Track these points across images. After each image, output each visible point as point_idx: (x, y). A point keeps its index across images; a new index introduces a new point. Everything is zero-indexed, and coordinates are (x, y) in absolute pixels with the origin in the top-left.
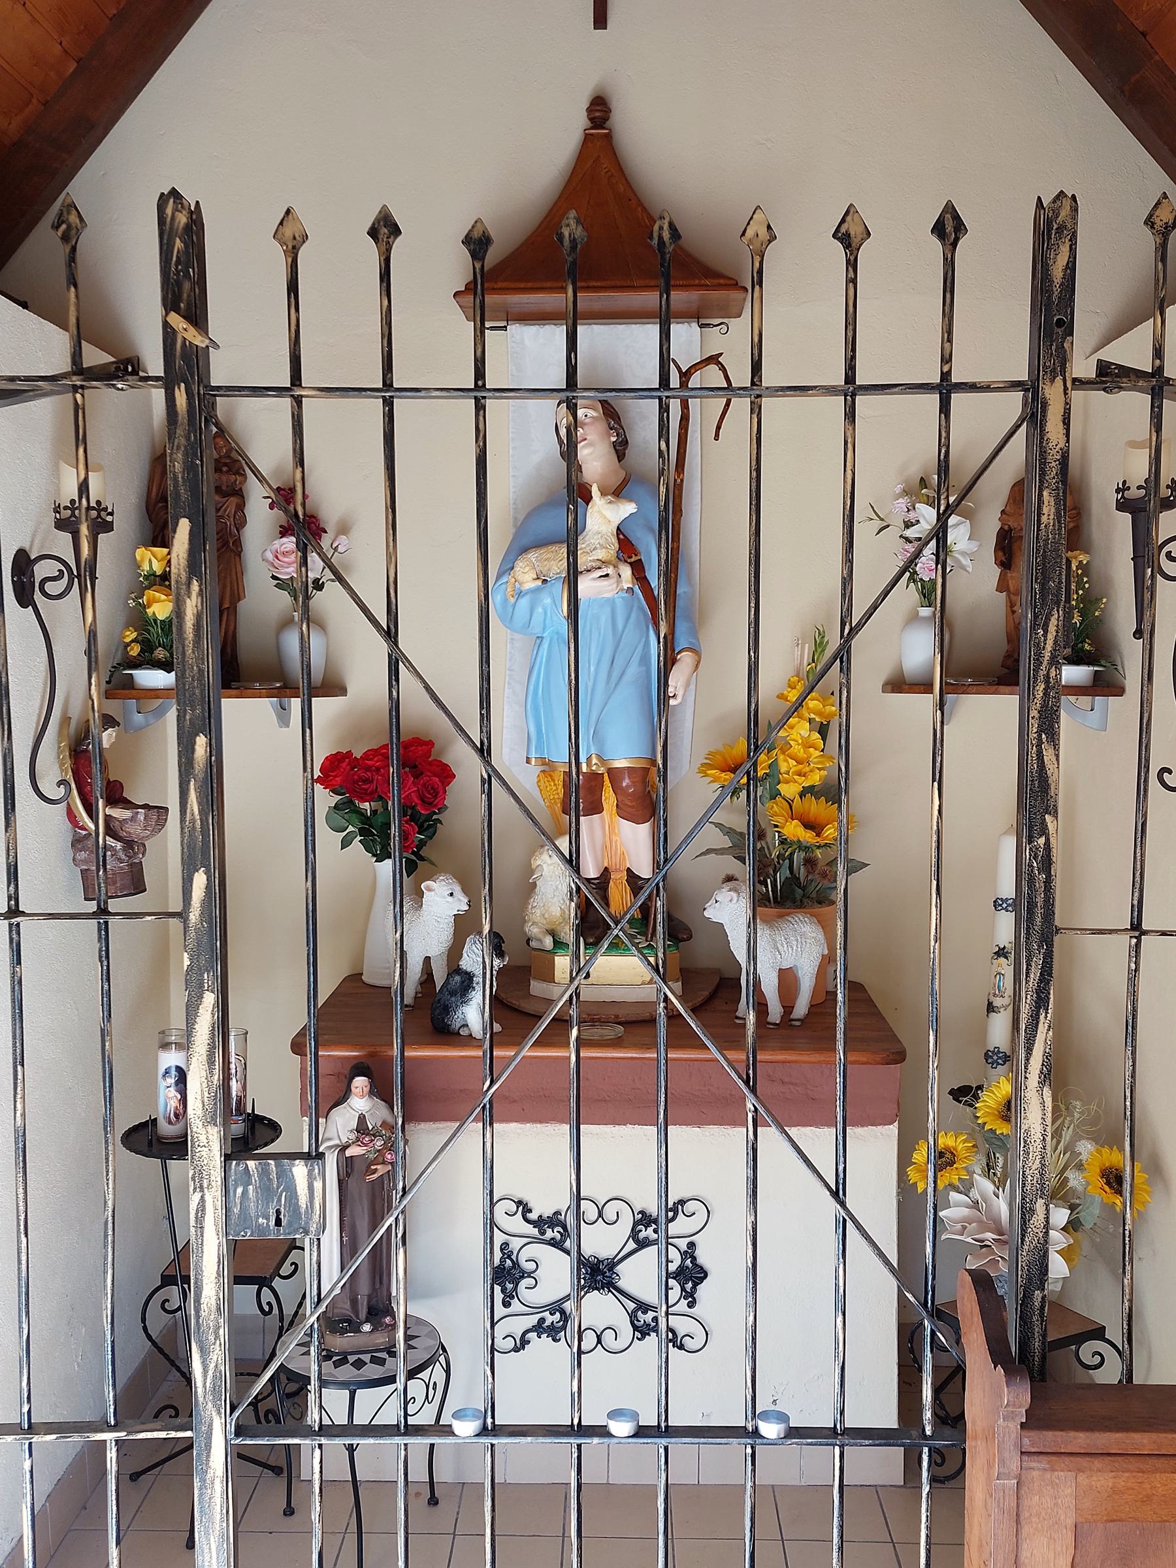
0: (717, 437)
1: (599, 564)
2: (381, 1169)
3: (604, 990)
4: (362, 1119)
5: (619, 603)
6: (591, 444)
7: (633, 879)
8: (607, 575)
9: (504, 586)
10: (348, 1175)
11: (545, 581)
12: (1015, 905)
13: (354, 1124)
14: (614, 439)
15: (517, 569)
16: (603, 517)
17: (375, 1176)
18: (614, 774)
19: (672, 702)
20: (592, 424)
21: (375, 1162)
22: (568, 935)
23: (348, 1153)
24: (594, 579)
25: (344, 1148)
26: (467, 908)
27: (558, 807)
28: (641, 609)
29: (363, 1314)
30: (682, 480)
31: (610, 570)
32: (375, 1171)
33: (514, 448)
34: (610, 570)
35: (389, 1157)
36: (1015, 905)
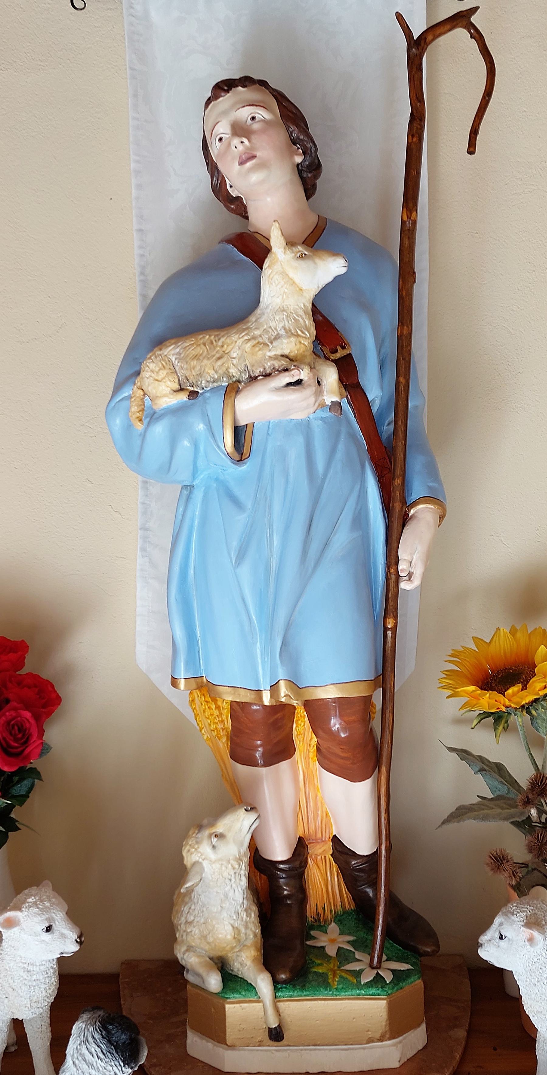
0: (471, 149)
1: (284, 363)
5: (318, 428)
6: (263, 166)
7: (340, 850)
8: (299, 382)
9: (126, 403)
11: (193, 395)
14: (299, 159)
15: (145, 374)
16: (292, 283)
18: (317, 711)
19: (403, 585)
20: (263, 131)
22: (247, 963)
24: (277, 389)
26: (75, 948)
27: (223, 745)
28: (352, 436)
30: (415, 223)
31: (304, 374)
33: (139, 187)
34: (304, 374)
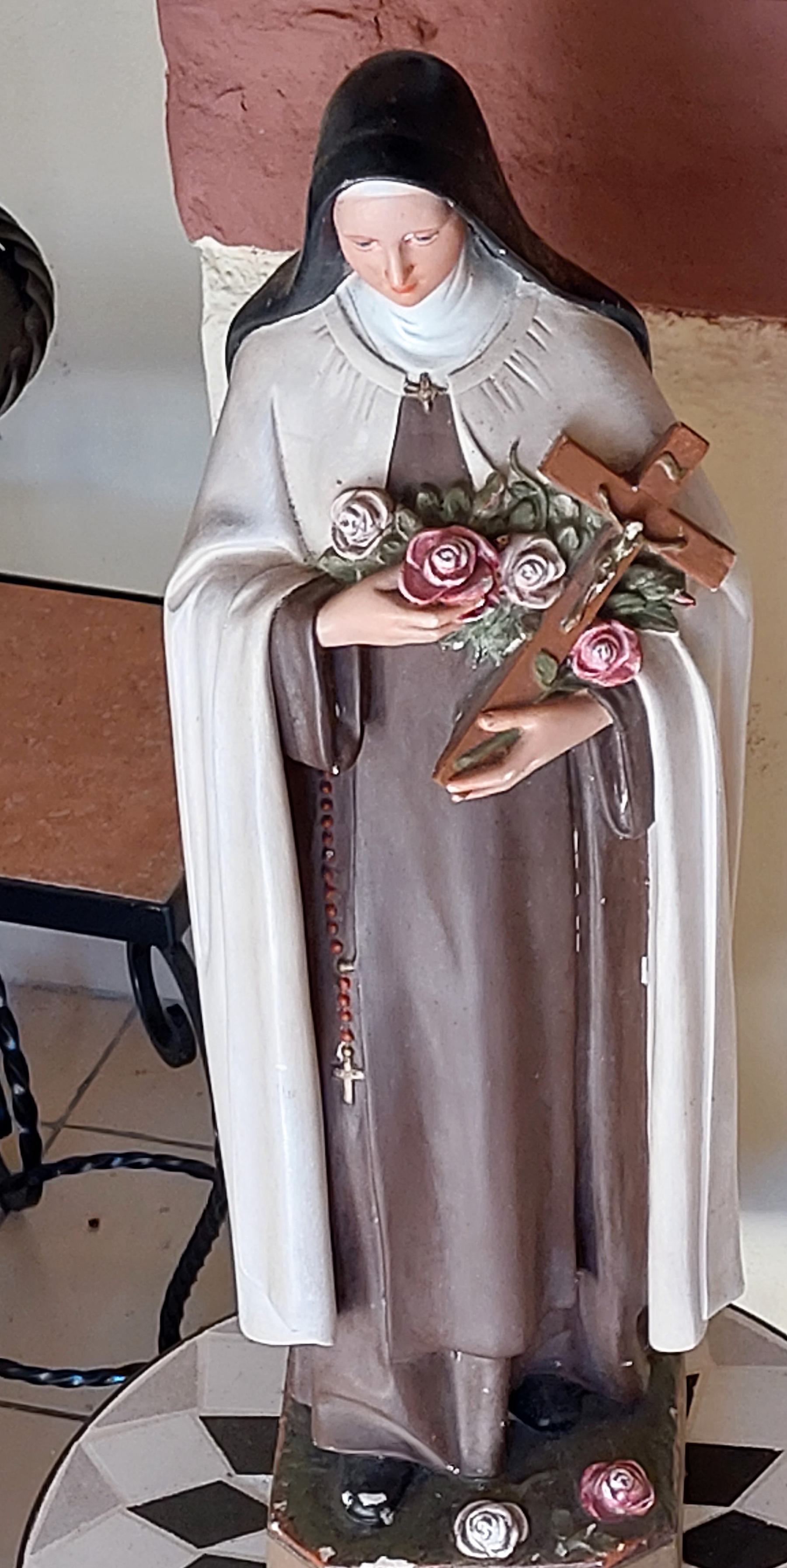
2: (542, 737)
3: (296, 710)
4: (425, 414)
10: (342, 743)
12: (77, 1527)
13: (373, 449)
17: (499, 781)
21: (499, 691)
23: (337, 626)
25: (315, 589)
29: (478, 1432)
32: (497, 753)
35: (597, 658)
36: (77, 1527)
